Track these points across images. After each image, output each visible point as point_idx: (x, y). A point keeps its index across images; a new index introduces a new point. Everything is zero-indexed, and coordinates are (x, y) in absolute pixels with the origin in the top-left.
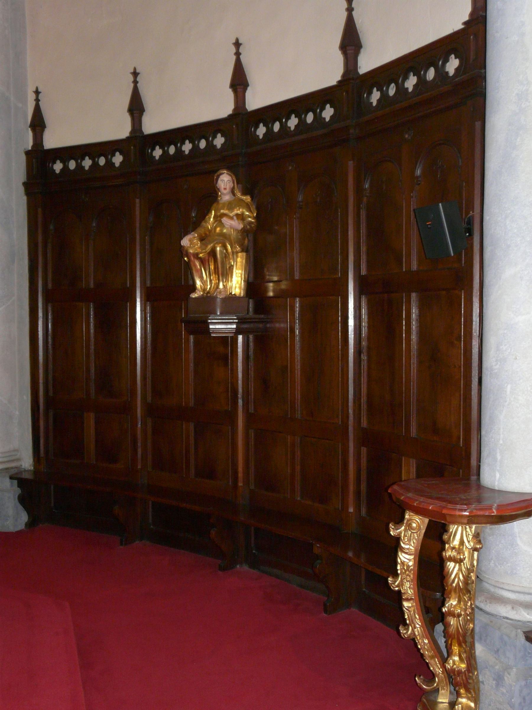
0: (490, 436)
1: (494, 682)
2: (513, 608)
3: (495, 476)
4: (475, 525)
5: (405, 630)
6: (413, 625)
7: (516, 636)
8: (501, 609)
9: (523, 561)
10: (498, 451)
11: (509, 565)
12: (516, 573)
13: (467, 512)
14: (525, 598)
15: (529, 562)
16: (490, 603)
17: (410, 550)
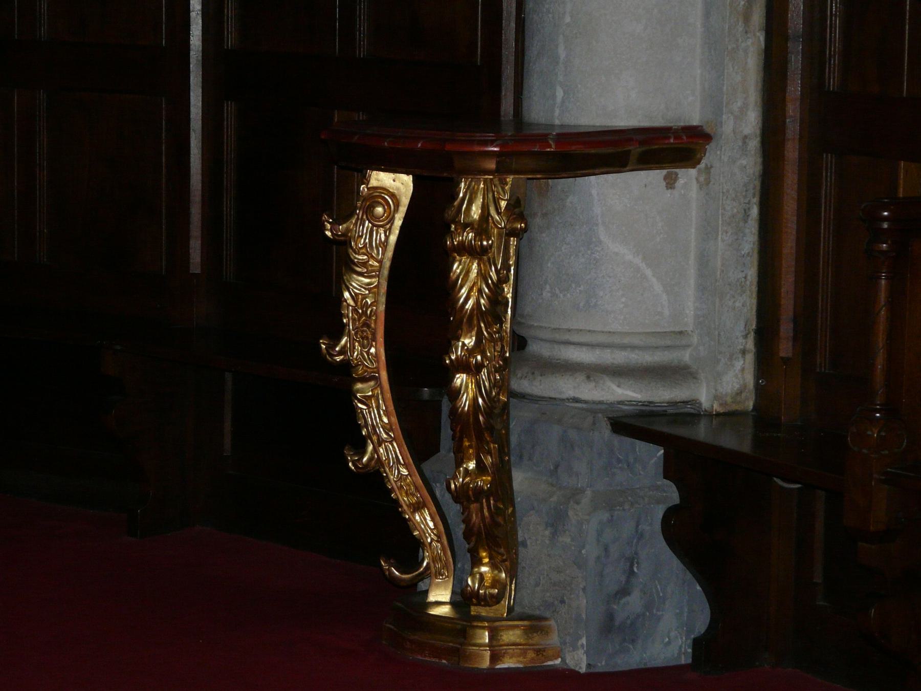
0: (545, 10)
1: (547, 533)
2: (588, 377)
3: (554, 96)
4: (512, 177)
5: (355, 454)
6: (375, 438)
7: (594, 423)
8: (565, 383)
9: (610, 277)
10: (561, 39)
11: (582, 288)
12: (596, 305)
13: (494, 144)
14: (614, 359)
15: (622, 279)
16: (541, 375)
17: (370, 269)
